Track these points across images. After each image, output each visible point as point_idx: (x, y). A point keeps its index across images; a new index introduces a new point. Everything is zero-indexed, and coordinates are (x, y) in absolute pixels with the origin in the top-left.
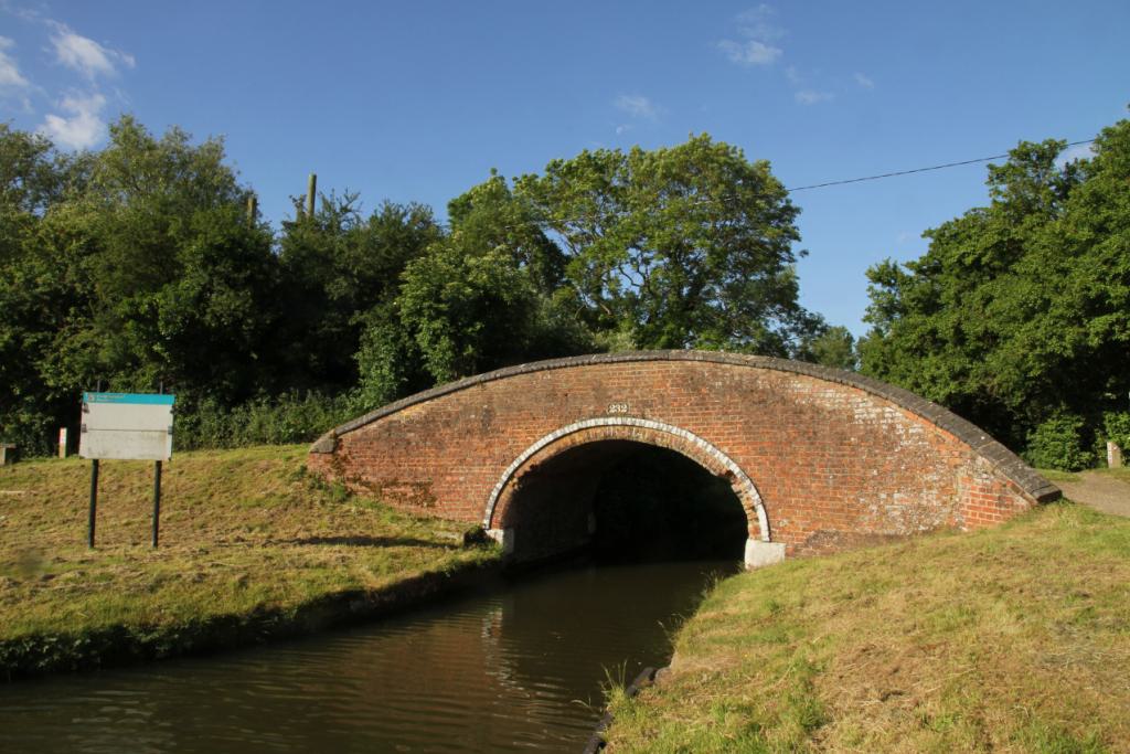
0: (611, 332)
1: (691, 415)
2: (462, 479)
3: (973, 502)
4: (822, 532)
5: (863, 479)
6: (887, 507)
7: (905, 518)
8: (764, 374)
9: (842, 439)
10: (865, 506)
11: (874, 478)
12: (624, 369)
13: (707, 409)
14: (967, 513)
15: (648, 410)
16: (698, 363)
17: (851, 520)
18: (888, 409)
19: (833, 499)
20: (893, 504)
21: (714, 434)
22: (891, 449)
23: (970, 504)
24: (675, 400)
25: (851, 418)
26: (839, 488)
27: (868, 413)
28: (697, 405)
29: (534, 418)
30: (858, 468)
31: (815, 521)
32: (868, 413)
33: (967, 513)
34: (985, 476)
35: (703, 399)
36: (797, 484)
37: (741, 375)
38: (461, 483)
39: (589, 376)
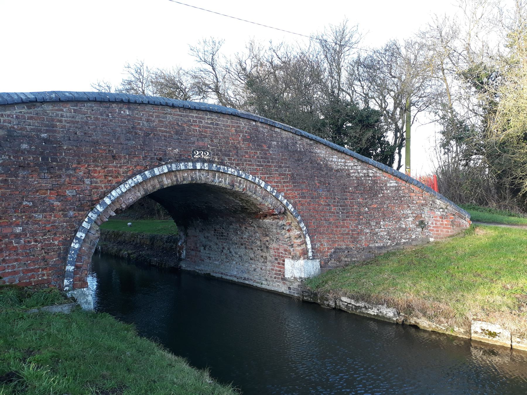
0: (474, 89)
1: (258, 166)
2: (19, 230)
3: (436, 224)
4: (338, 248)
5: (359, 213)
6: (377, 230)
7: (390, 236)
8: (300, 140)
9: (344, 189)
10: (362, 230)
11: (366, 213)
12: (204, 119)
13: (269, 162)
14: (433, 230)
15: (226, 158)
16: (259, 124)
17: (355, 240)
18: (370, 171)
19: (343, 227)
20: (381, 228)
21: (275, 182)
22: (376, 195)
23: (434, 225)
24: (246, 153)
25: (349, 175)
26: (345, 220)
27: (358, 173)
28: (262, 158)
29: (114, 157)
30: (355, 207)
31: (334, 242)
32: (358, 173)
33: (433, 230)
34: (441, 210)
35: (266, 154)
36: (323, 218)
37: (287, 139)
38: (18, 236)
39: (170, 118)
